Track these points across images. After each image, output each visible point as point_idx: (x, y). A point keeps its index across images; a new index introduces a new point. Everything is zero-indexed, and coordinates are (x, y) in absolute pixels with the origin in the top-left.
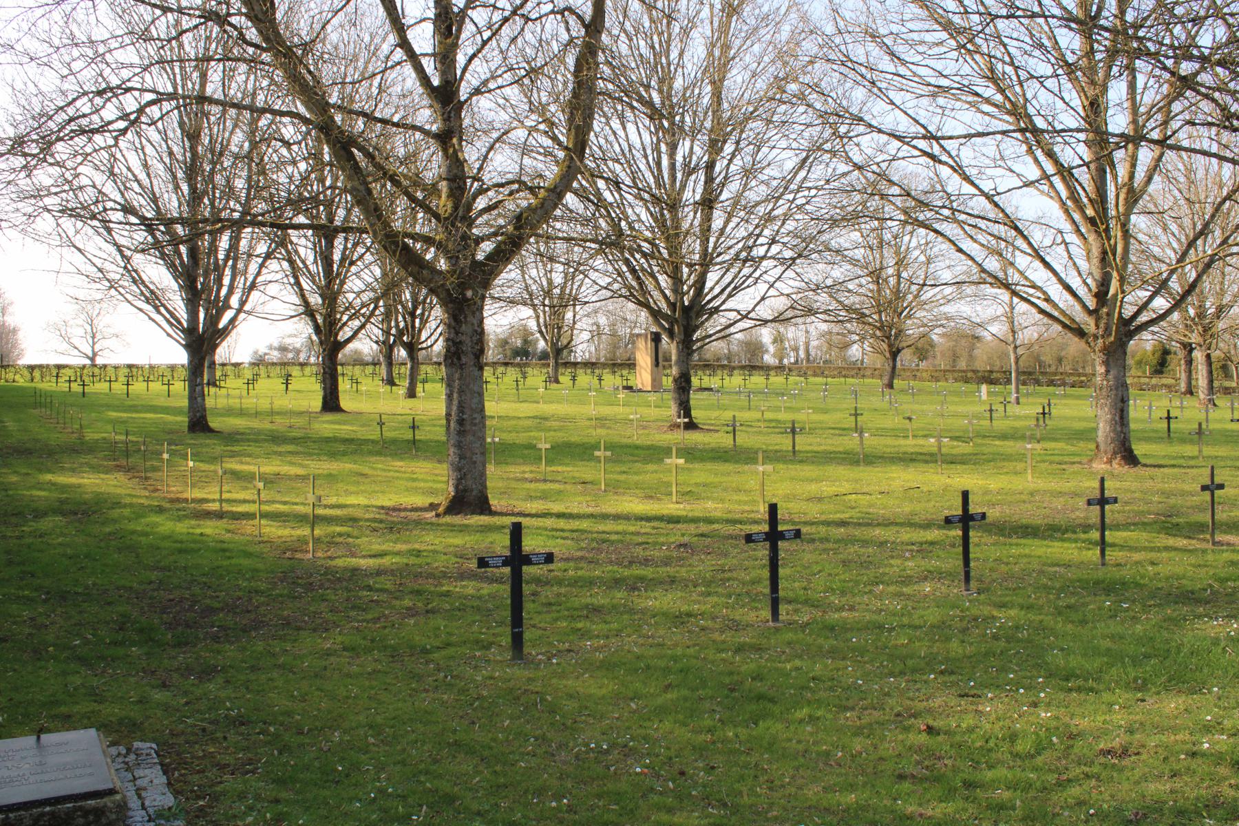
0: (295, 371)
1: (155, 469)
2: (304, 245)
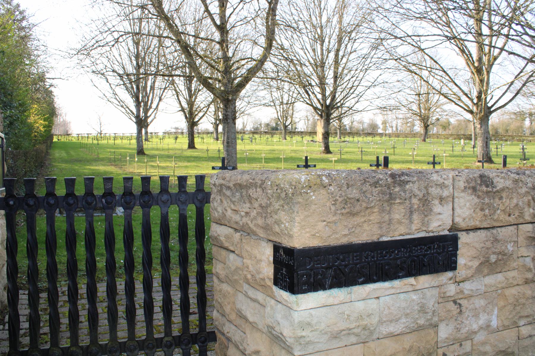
0: (180, 136)
1: (124, 165)
2: (180, 83)
